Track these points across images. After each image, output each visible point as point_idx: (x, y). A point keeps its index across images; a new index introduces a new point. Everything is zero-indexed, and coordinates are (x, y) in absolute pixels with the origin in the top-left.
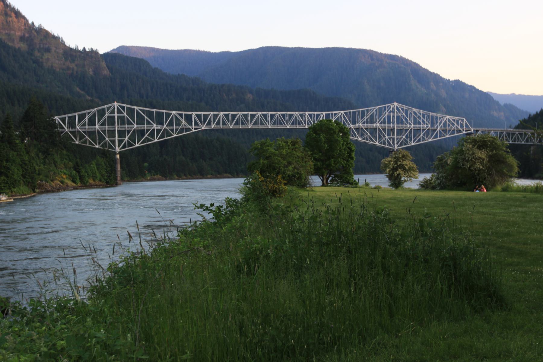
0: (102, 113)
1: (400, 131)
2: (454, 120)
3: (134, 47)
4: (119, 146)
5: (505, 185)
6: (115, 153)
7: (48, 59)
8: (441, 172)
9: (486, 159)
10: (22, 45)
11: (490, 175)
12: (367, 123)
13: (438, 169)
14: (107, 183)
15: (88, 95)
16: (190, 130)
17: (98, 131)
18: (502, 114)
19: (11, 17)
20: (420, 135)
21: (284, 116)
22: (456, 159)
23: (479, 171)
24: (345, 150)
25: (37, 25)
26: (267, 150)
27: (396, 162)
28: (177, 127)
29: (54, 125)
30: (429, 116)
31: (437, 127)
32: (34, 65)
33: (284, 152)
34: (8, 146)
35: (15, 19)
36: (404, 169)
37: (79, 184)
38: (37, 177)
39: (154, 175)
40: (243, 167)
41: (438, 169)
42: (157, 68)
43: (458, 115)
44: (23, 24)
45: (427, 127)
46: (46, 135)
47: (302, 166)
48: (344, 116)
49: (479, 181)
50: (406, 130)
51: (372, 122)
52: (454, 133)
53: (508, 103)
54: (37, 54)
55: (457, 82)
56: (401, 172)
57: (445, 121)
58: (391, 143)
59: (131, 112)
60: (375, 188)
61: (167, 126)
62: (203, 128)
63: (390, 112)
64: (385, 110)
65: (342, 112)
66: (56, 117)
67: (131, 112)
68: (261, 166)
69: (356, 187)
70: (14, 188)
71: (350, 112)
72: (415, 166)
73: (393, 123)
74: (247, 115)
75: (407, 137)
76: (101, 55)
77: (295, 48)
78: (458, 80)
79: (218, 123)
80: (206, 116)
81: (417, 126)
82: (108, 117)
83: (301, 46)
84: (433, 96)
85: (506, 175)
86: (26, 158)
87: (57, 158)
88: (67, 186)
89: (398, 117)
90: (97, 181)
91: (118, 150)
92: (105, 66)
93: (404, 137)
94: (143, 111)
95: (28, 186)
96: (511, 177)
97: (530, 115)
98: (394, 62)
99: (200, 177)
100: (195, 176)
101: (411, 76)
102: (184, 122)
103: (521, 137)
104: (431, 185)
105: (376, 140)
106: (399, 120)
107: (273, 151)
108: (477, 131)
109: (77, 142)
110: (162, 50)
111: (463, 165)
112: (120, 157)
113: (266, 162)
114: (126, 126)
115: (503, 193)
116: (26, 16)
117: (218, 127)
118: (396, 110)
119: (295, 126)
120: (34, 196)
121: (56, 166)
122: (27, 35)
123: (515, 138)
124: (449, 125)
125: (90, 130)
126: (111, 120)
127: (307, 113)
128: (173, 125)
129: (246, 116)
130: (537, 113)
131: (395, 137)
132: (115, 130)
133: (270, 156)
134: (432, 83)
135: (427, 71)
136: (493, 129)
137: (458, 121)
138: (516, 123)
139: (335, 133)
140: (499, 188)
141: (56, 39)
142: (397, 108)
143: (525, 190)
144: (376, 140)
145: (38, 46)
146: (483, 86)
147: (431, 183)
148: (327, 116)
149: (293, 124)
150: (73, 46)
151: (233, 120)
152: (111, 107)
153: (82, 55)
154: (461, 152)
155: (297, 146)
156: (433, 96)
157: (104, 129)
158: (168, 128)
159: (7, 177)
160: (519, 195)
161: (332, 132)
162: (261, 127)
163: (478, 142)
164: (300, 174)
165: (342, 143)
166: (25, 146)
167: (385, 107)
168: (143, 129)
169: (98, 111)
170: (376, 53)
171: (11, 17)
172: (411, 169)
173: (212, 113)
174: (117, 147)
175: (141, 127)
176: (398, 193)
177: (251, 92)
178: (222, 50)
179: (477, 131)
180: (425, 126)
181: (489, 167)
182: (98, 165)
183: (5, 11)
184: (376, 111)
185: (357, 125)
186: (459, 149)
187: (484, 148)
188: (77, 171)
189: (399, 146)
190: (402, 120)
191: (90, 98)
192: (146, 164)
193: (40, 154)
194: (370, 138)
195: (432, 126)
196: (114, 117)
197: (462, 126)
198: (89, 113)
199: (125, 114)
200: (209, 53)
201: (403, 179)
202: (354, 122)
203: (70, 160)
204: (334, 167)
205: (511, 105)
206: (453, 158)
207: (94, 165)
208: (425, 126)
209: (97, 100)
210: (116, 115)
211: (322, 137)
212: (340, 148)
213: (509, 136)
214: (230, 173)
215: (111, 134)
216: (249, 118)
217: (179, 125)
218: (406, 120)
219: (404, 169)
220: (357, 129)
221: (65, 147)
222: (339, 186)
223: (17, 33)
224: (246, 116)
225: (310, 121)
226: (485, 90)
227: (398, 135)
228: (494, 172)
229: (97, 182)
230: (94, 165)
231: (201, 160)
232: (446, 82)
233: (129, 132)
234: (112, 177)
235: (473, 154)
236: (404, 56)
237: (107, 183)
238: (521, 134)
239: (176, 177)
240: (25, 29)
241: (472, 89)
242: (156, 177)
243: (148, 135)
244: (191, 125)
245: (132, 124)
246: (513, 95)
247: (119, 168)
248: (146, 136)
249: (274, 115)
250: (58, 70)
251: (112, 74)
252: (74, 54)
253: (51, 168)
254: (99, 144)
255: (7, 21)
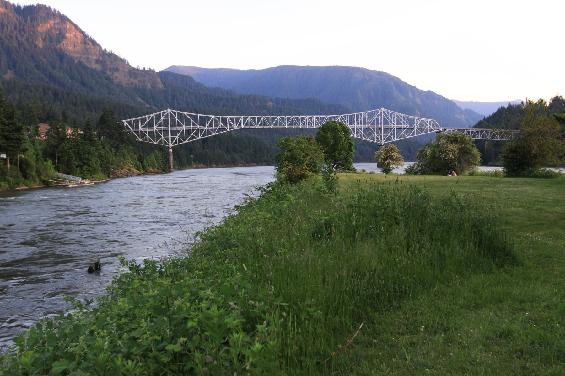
0: (158, 117)
1: (386, 130)
2: (427, 122)
3: (182, 66)
4: (172, 143)
5: (471, 171)
6: (169, 148)
7: (117, 77)
8: (422, 161)
9: (457, 151)
10: (97, 66)
11: (459, 163)
12: (361, 124)
13: (420, 159)
14: (163, 170)
15: (148, 104)
16: (225, 129)
17: (156, 131)
18: (463, 116)
19: (89, 45)
20: (401, 132)
21: (297, 118)
22: (433, 151)
23: (451, 160)
24: (346, 144)
25: (108, 51)
26: (290, 145)
27: (386, 154)
28: (216, 128)
29: (122, 127)
30: (408, 118)
31: (415, 126)
32: (107, 81)
33: (303, 146)
34: (89, 143)
35: (92, 47)
36: (393, 159)
37: (142, 171)
38: (110, 166)
39: (198, 164)
40: (266, 158)
41: (420, 159)
42: (200, 83)
43: (430, 118)
44: (98, 50)
45: (407, 127)
46: (117, 134)
47: (317, 157)
48: (343, 118)
49: (451, 168)
50: (391, 129)
51: (364, 123)
52: (427, 132)
53: (468, 108)
54: (109, 73)
55: (429, 92)
56: (391, 161)
57: (421, 123)
58: (379, 139)
59: (180, 116)
60: (370, 173)
61: (208, 127)
62: (236, 128)
63: (378, 116)
64: (375, 114)
65: (342, 115)
66: (124, 121)
67: (180, 116)
68: (285, 156)
69: (356, 173)
70: (94, 174)
71: (348, 116)
72: (401, 157)
73: (381, 124)
74: (269, 118)
75: (390, 134)
76: (157, 73)
77: (305, 66)
78: (430, 91)
79: (247, 125)
80: (238, 119)
81: (399, 126)
82: (163, 120)
83: (309, 65)
84: (411, 103)
85: (472, 163)
86: (103, 152)
87: (125, 151)
88: (133, 173)
89: (384, 119)
90: (155, 169)
91: (171, 145)
92: (160, 81)
93: (389, 134)
94: (190, 115)
95: (104, 173)
96: (476, 165)
97: (485, 117)
98: (380, 77)
99: (233, 165)
100: (229, 165)
101: (394, 88)
102: (221, 124)
103: (478, 134)
104: (414, 171)
105: (368, 137)
106: (386, 122)
107: (294, 145)
108: (445, 130)
109: (140, 140)
110: (204, 69)
111: (439, 156)
112: (173, 150)
113: (289, 153)
114: (177, 127)
115: (470, 177)
116: (100, 44)
117: (247, 127)
118: (383, 114)
119: (305, 126)
120: (109, 180)
121: (124, 158)
122: (101, 58)
123: (483, 135)
124: (423, 125)
125: (150, 130)
126: (166, 123)
127: (315, 116)
128: (212, 126)
129: (268, 119)
130: (490, 116)
131: (382, 134)
132: (168, 130)
133: (292, 149)
134: (410, 93)
135: (406, 84)
136: (457, 128)
137: (430, 122)
138: (474, 123)
139: (339, 131)
140: (467, 173)
141: (123, 61)
142: (384, 113)
143: (487, 174)
144: (368, 137)
145: (109, 67)
146: (449, 95)
147: (413, 170)
148: (330, 118)
149: (304, 124)
150: (136, 67)
151: (258, 122)
152: (165, 113)
153: (143, 73)
154: (438, 146)
155: (312, 141)
156: (411, 103)
157: (160, 130)
158: (209, 128)
159: (89, 166)
160: (484, 178)
161: (337, 130)
162: (279, 127)
163: (450, 138)
164: (315, 163)
165: (344, 139)
166: (102, 142)
167: (375, 112)
168: (189, 129)
169: (156, 115)
170: (367, 70)
171: (89, 45)
172: (398, 159)
173: (242, 117)
174: (170, 143)
175: (188, 128)
176: (389, 177)
177: (271, 100)
178: (249, 69)
179: (445, 130)
180: (405, 126)
181: (459, 157)
182: (156, 156)
183: (85, 40)
184: (368, 114)
185: (353, 125)
186: (436, 143)
187: (455, 143)
188: (140, 162)
189: (385, 141)
190: (387, 121)
191: (148, 106)
192: (192, 156)
193: (113, 148)
194: (363, 135)
195: (410, 126)
196: (168, 120)
197: (433, 126)
198: (149, 117)
199: (176, 118)
200: (239, 71)
201: (391, 167)
202: (351, 124)
203: (135, 153)
204: (338, 157)
205: (470, 110)
206: (432, 150)
207: (153, 157)
208: (405, 126)
209: (154, 107)
210: (169, 118)
211: (329, 134)
212: (343, 143)
213: (469, 134)
214: (256, 162)
215: (166, 133)
216: (270, 121)
217: (217, 126)
218: (390, 121)
219: (393, 159)
220: (353, 129)
221: (131, 144)
222: (342, 172)
223: (93, 57)
224: (254, 119)
225: (317, 123)
226: (450, 98)
227: (384, 133)
228: (463, 161)
229: (156, 170)
230: (153, 157)
231: (234, 152)
232: (420, 93)
233: (179, 131)
234: (167, 166)
235: (447, 147)
236: (388, 72)
237: (163, 170)
238: (478, 132)
239: (215, 166)
240: (100, 54)
241: (440, 98)
242: (199, 166)
243: (194, 134)
244: (226, 126)
245: (181, 126)
246: (472, 102)
247: (172, 159)
248: (192, 134)
249: (290, 118)
250: (124, 85)
251: (165, 87)
252: (137, 72)
253: (121, 160)
254: (157, 141)
255: (86, 49)
